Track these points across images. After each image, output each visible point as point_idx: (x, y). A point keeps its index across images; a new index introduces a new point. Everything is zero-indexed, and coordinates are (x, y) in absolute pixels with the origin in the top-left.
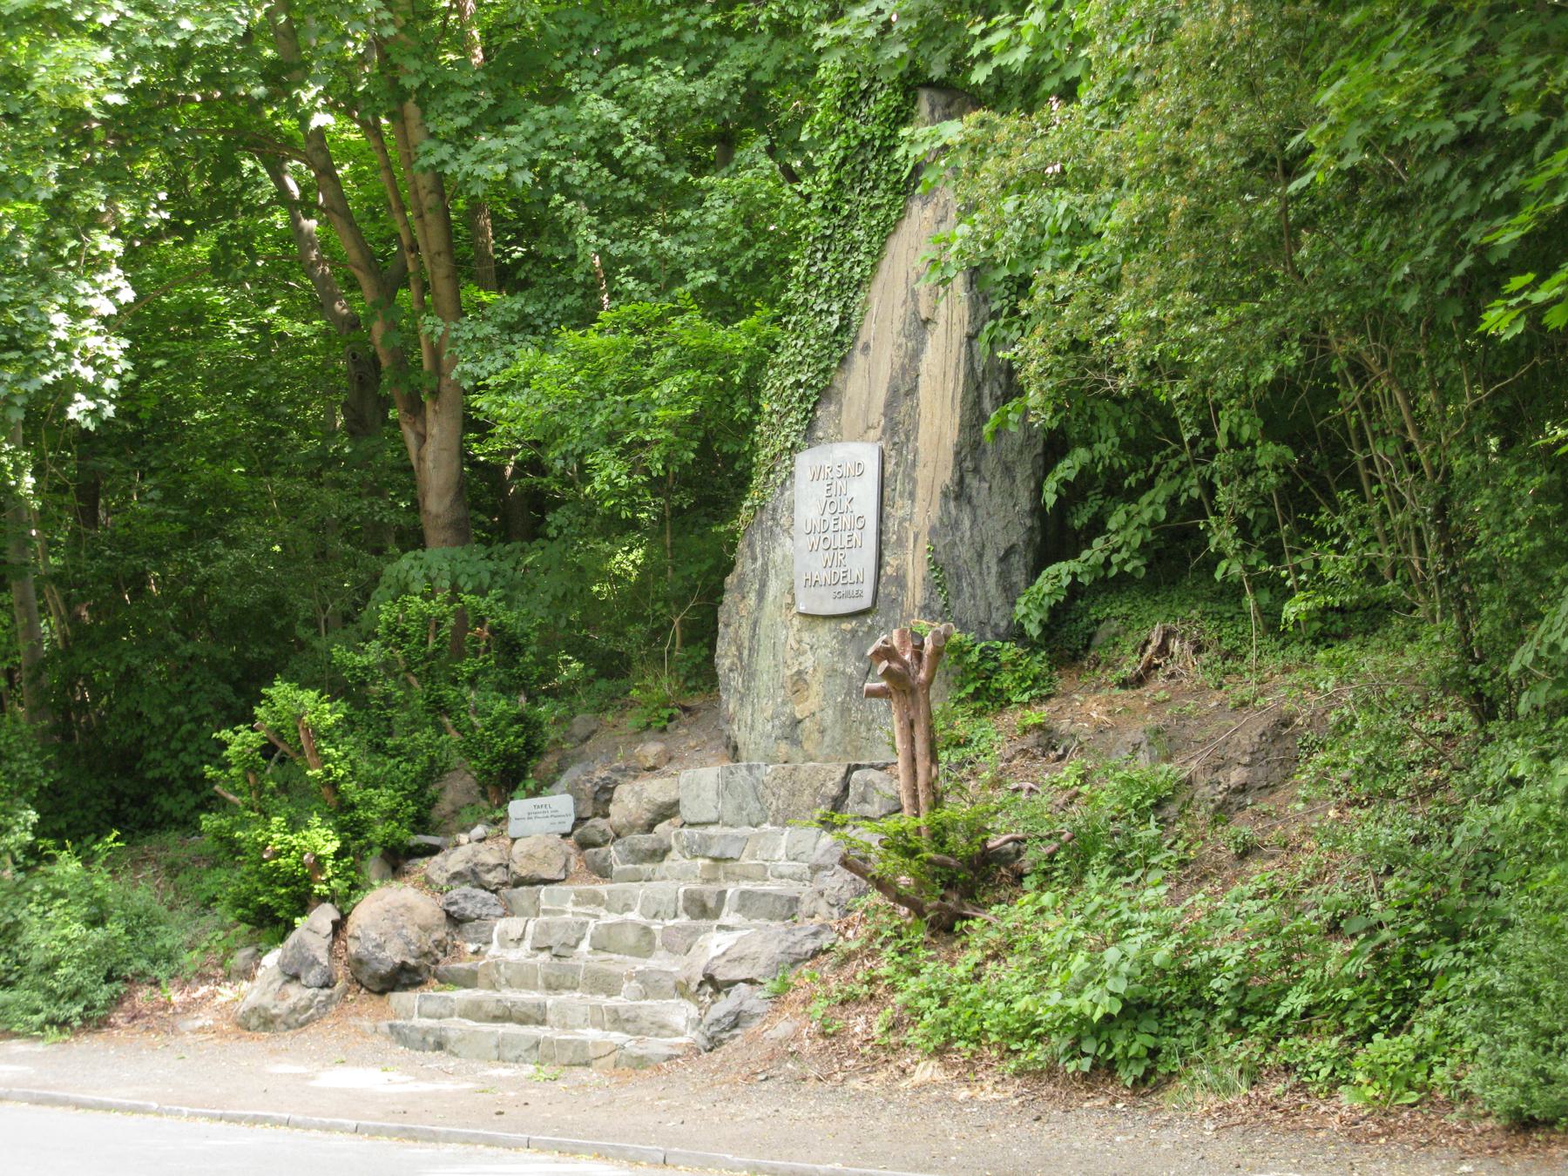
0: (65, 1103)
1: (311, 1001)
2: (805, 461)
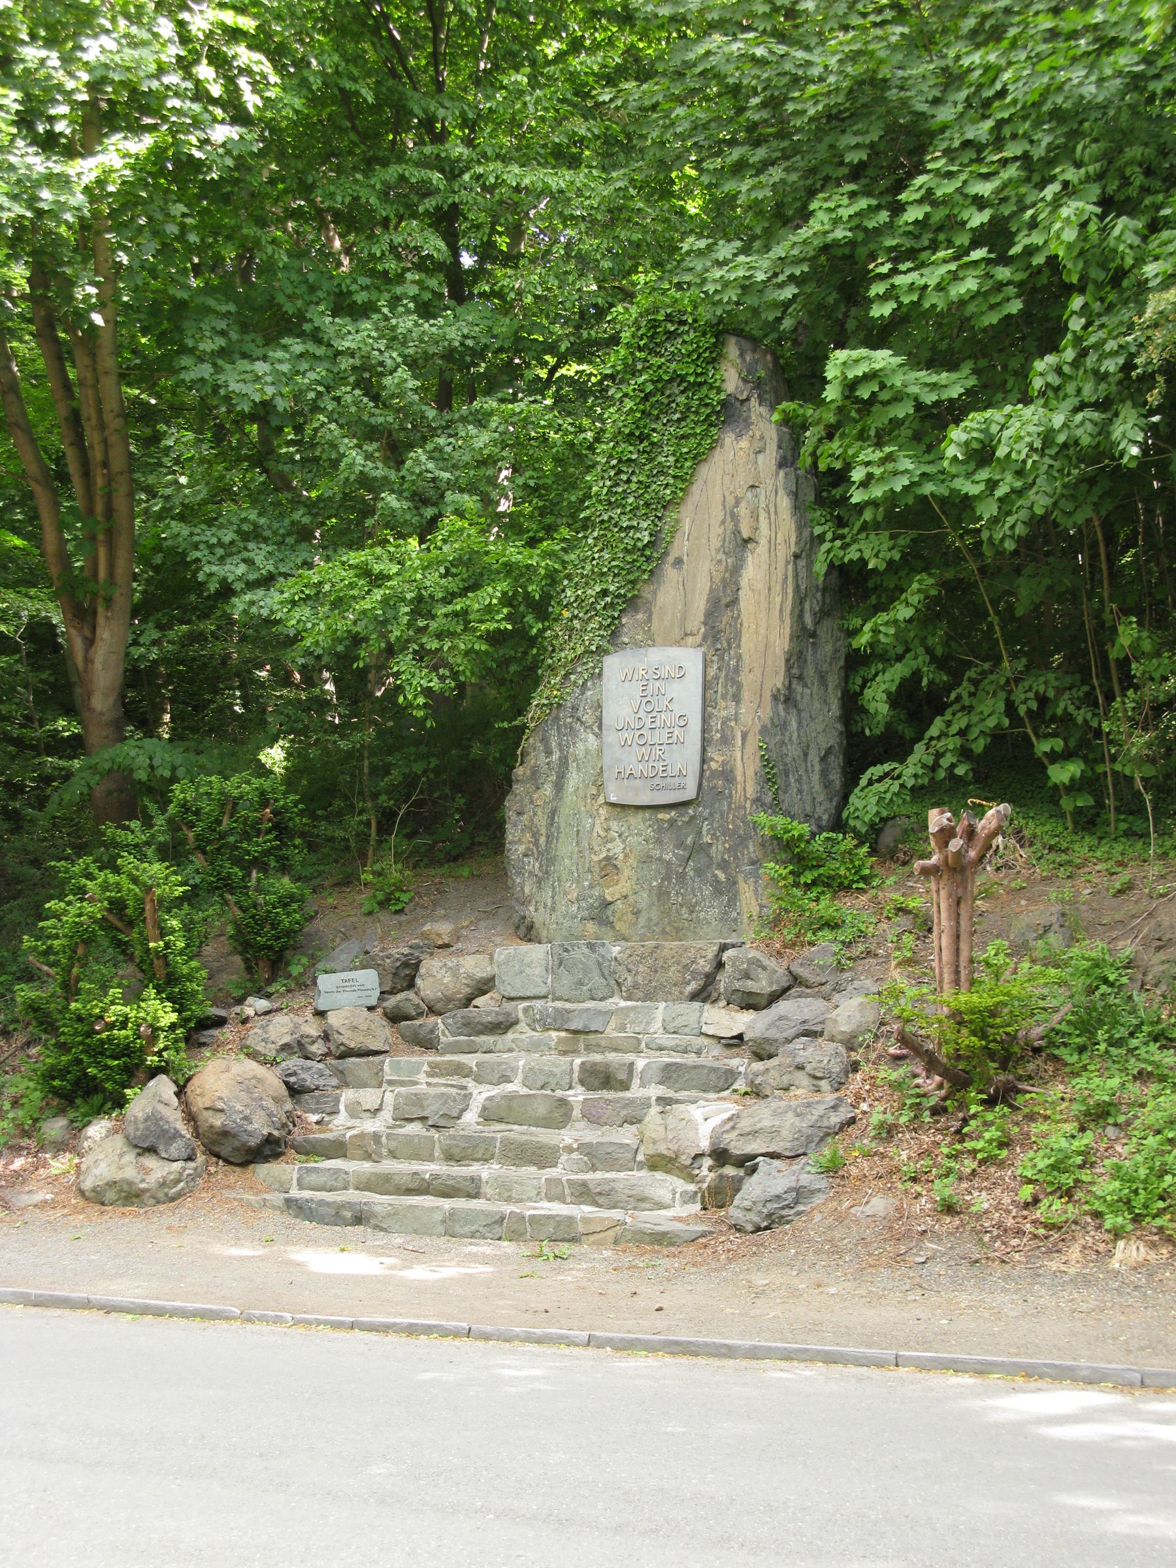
0: (87, 1305)
1: (181, 1174)
2: (613, 664)
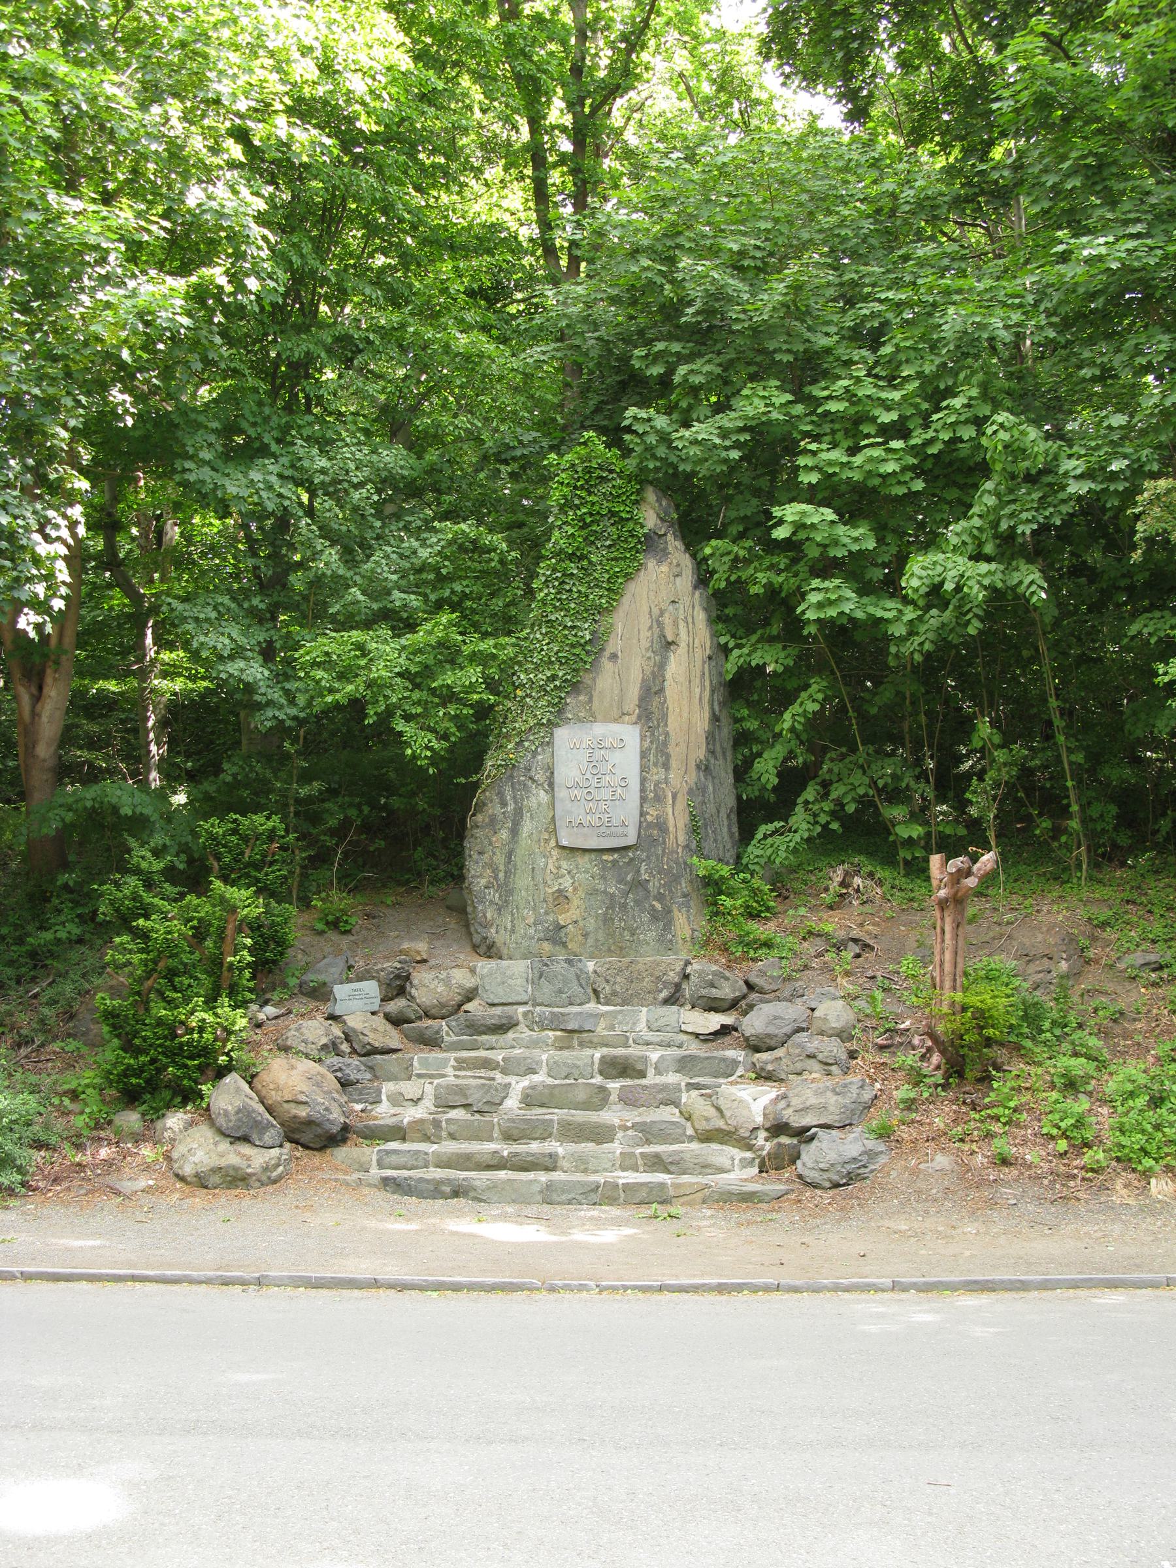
2: (562, 735)
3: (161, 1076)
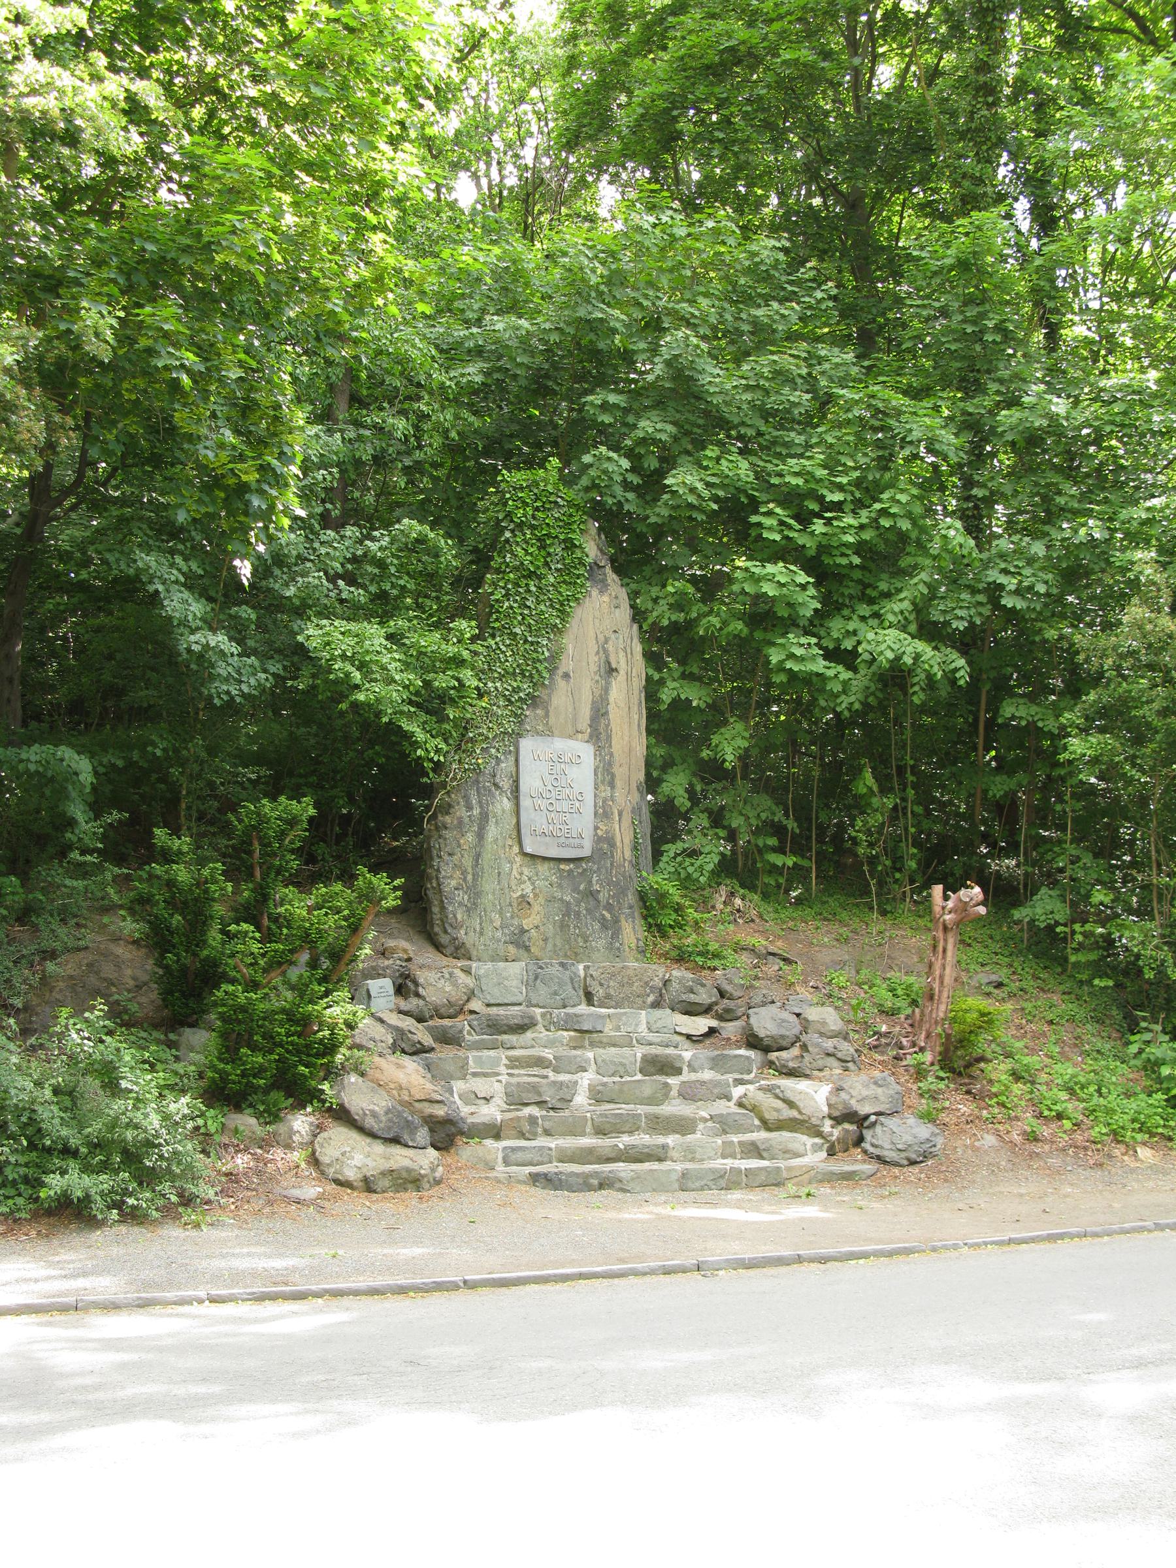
3: (273, 1073)
